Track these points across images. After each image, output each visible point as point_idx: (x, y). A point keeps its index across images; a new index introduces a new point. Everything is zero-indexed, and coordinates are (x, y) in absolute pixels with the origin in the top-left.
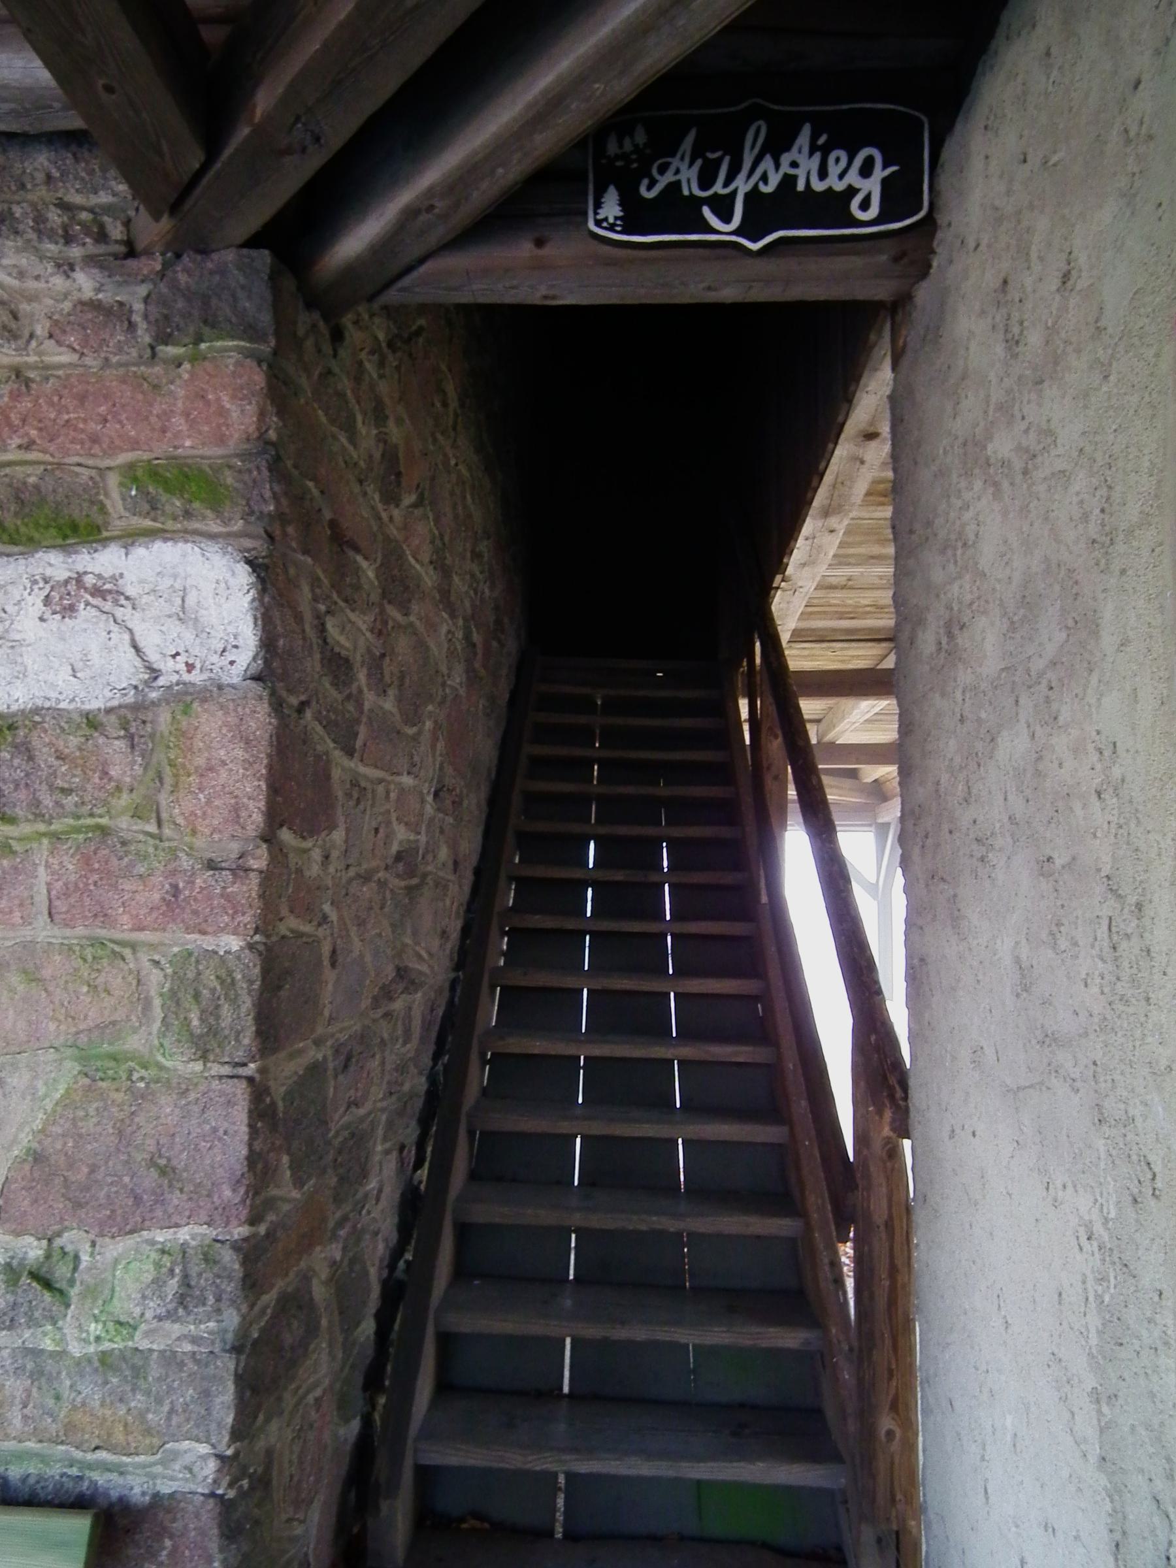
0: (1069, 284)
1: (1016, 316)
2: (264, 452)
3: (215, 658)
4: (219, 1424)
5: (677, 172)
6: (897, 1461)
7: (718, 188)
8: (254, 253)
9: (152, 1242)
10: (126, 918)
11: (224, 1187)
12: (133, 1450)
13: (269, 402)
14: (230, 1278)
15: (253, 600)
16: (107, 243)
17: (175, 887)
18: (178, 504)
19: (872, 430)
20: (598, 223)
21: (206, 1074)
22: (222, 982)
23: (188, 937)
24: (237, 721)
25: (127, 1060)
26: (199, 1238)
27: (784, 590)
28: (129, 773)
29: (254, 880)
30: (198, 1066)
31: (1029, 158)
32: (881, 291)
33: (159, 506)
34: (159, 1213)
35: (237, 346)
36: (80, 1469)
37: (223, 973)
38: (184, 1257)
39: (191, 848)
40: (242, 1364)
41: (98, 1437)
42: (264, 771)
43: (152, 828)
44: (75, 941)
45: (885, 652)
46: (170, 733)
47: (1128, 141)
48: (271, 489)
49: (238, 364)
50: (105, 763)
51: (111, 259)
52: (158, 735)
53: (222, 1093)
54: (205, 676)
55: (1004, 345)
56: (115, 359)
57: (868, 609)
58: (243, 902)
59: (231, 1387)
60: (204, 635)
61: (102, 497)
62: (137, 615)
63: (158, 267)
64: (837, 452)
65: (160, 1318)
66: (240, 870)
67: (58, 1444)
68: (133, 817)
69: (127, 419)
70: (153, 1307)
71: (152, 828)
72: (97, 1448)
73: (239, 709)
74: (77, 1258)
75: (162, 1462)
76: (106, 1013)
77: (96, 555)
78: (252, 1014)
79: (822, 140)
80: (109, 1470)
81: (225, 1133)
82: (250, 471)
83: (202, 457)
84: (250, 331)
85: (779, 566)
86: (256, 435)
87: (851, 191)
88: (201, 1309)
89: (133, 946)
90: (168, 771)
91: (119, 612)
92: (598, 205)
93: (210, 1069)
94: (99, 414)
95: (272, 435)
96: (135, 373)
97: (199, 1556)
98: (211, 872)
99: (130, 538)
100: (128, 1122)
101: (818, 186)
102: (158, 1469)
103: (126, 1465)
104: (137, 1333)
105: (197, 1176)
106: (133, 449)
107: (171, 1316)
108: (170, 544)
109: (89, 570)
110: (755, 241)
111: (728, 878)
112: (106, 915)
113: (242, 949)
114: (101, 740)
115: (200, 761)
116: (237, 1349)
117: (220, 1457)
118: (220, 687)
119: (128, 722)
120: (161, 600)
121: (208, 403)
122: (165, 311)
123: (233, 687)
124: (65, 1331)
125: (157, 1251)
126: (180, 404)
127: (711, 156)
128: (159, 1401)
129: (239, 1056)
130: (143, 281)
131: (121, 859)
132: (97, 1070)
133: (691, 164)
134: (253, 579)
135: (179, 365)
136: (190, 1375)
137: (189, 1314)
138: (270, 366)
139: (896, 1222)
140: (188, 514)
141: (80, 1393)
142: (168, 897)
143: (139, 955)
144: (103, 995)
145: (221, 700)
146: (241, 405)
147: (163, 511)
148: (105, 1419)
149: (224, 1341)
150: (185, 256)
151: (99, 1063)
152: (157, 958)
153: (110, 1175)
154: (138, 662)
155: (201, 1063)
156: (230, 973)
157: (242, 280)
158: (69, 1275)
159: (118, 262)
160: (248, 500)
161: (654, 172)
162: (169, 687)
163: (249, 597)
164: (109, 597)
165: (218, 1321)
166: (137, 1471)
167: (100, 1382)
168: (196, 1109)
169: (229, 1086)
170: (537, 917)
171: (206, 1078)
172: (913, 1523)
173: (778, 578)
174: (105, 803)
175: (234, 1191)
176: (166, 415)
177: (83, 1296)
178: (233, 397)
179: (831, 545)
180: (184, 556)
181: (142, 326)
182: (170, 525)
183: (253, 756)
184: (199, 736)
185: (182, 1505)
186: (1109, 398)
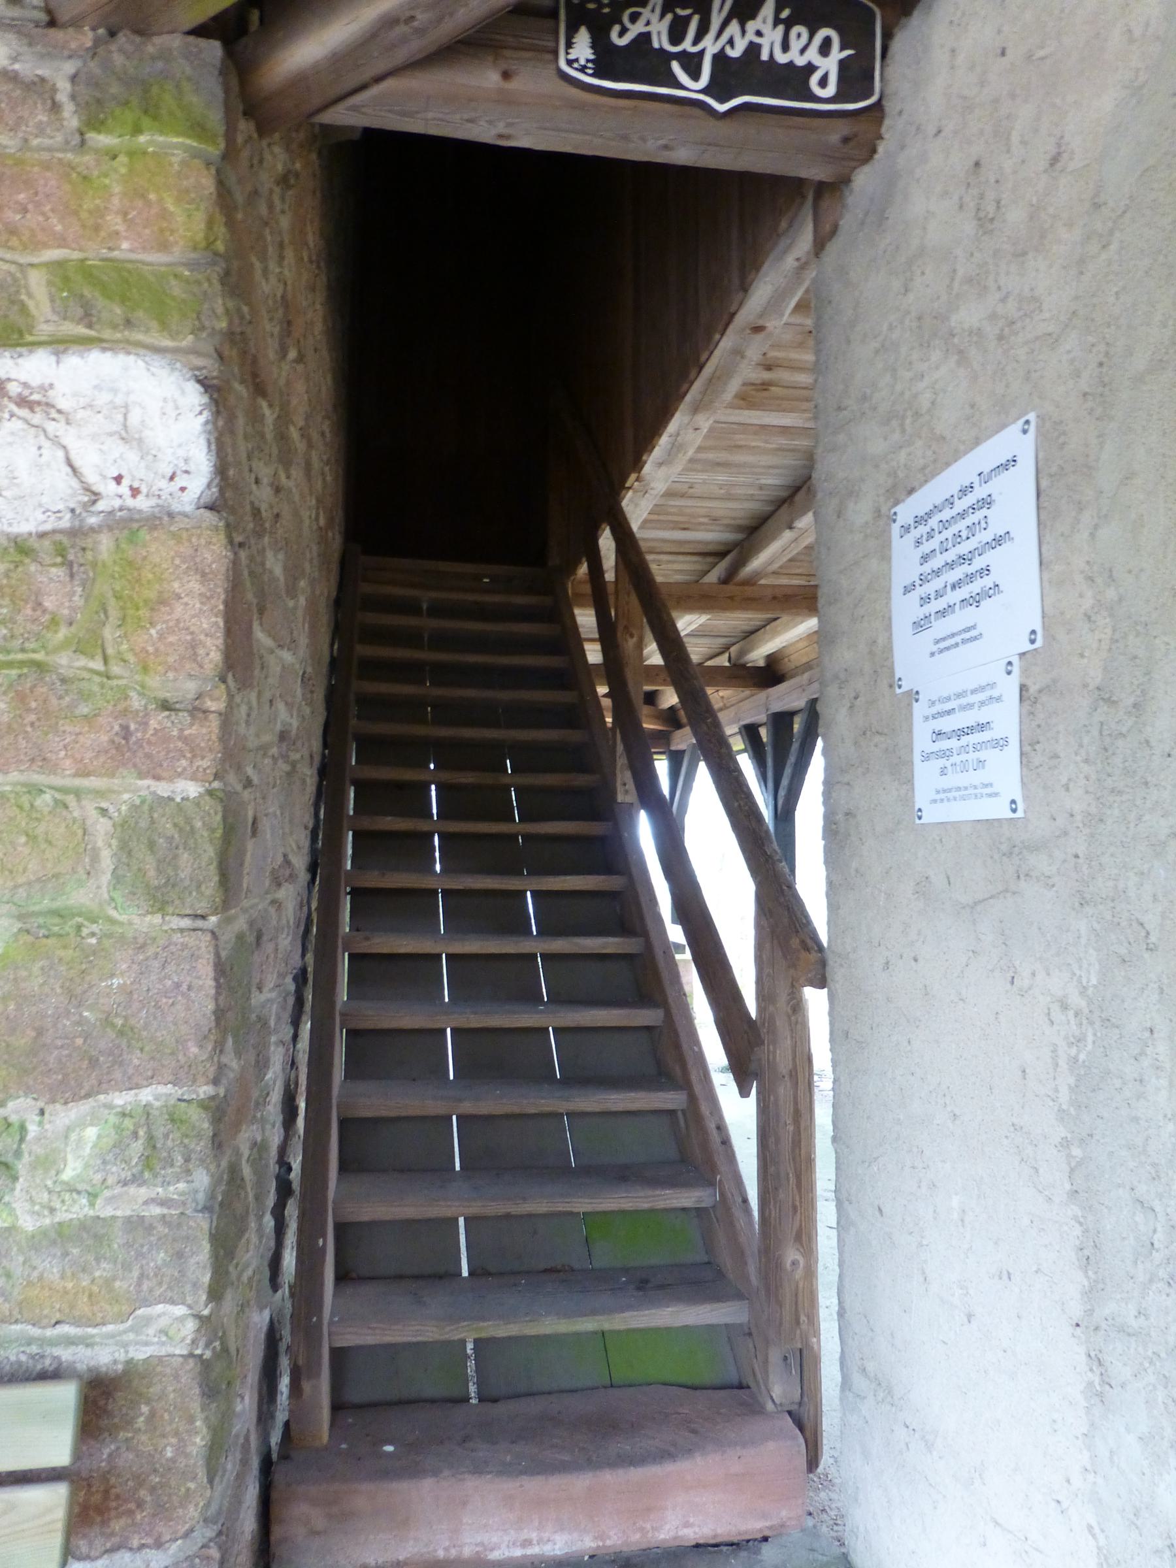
0: (1059, 166)
1: (991, 195)
2: (214, 264)
3: (163, 484)
4: (195, 1285)
5: (648, 23)
6: (801, 1285)
7: (687, 45)
8: (203, 43)
9: (109, 1106)
10: (68, 762)
11: (190, 1044)
12: (99, 1320)
13: (217, 210)
14: (199, 1136)
15: (207, 423)
16: (23, 7)
17: (125, 728)
18: (118, 311)
19: (760, 323)
20: (570, 63)
21: (165, 928)
22: (181, 830)
23: (140, 783)
24: (190, 551)
25: (73, 915)
26: (164, 1098)
27: (636, 491)
28: (67, 604)
29: (214, 723)
30: (157, 919)
31: (1008, 52)
32: (816, 172)
33: (94, 312)
34: (118, 1074)
35: (183, 144)
36: (41, 1346)
37: (180, 821)
38: (148, 1118)
39: (143, 687)
40: (214, 1224)
41: (60, 1310)
42: (221, 607)
43: (97, 665)
44: (8, 788)
45: (705, 568)
46: (115, 562)
47: (1131, 41)
48: (224, 304)
49: (183, 163)
50: (38, 593)
51: (32, 25)
52: (100, 564)
53: (184, 946)
54: (153, 502)
55: (975, 222)
56: (35, 142)
57: (702, 520)
58: (203, 745)
59: (206, 1246)
60: (150, 458)
61: (23, 297)
62: (72, 430)
63: (89, 44)
64: (722, 344)
65: (125, 1183)
66: (197, 711)
67: (11, 1324)
68: (75, 652)
69: (53, 210)
70: (116, 1171)
71: (97, 665)
72: (57, 1323)
73: (194, 540)
74: (23, 1128)
75: (132, 1329)
76: (49, 865)
77: (20, 361)
78: (215, 864)
79: (785, 14)
80: (73, 1343)
81: (190, 988)
82: (198, 283)
83: (144, 263)
84: (198, 129)
85: (638, 465)
86: (203, 244)
87: (810, 68)
88: (170, 1171)
89: (78, 793)
90: (112, 603)
91: (51, 427)
92: (569, 45)
93: (170, 922)
94: (17, 202)
95: (220, 246)
96: (60, 159)
97: (180, 1417)
98: (167, 713)
99: (60, 344)
100: (78, 980)
101: (782, 58)
102: (131, 1336)
103: (93, 1336)
104: (98, 1202)
105: (158, 1034)
106: (59, 247)
107: (137, 1180)
108: (109, 354)
109: (13, 376)
110: (722, 101)
111: (581, 780)
112: (44, 759)
113: (201, 795)
114: (33, 568)
115: (152, 595)
116: (206, 1209)
117: (198, 1317)
118: (171, 515)
119: (64, 549)
120: (99, 416)
121: (148, 204)
122: (98, 95)
123: (186, 515)
124: (14, 1205)
125: (117, 1114)
126: (116, 201)
127: (681, 12)
128: (126, 1267)
129: (202, 907)
130: (70, 57)
131: (61, 698)
132: (39, 927)
133: (662, 16)
134: (205, 399)
135: (114, 157)
136: (159, 1239)
137: (155, 1176)
138: (218, 171)
139: (799, 1069)
140: (128, 323)
141: (35, 1268)
142: (117, 739)
143: (84, 803)
144: (43, 846)
145: (172, 529)
146: (188, 210)
147: (99, 319)
148: (66, 1292)
149: (195, 1200)
150: (120, 34)
151: (41, 920)
152: (104, 805)
153: (61, 1038)
154: (75, 483)
155: (159, 916)
156: (188, 820)
157: (188, 70)
158: (15, 1146)
159: (39, 30)
160: (199, 314)
161: (626, 19)
162: (111, 513)
163: (202, 419)
164: (37, 409)
165: (188, 1182)
166: (105, 1341)
167: (59, 1254)
168: (156, 964)
169: (191, 940)
170: (389, 818)
171: (166, 931)
172: (815, 1340)
173: (633, 476)
174: (38, 637)
175: (201, 1047)
176: (99, 212)
177: (33, 1167)
178: (178, 201)
179: (694, 440)
180: (126, 369)
181: (68, 109)
182: (107, 334)
183: (210, 590)
184: (148, 567)
185: (159, 1369)
186: (1109, 265)
